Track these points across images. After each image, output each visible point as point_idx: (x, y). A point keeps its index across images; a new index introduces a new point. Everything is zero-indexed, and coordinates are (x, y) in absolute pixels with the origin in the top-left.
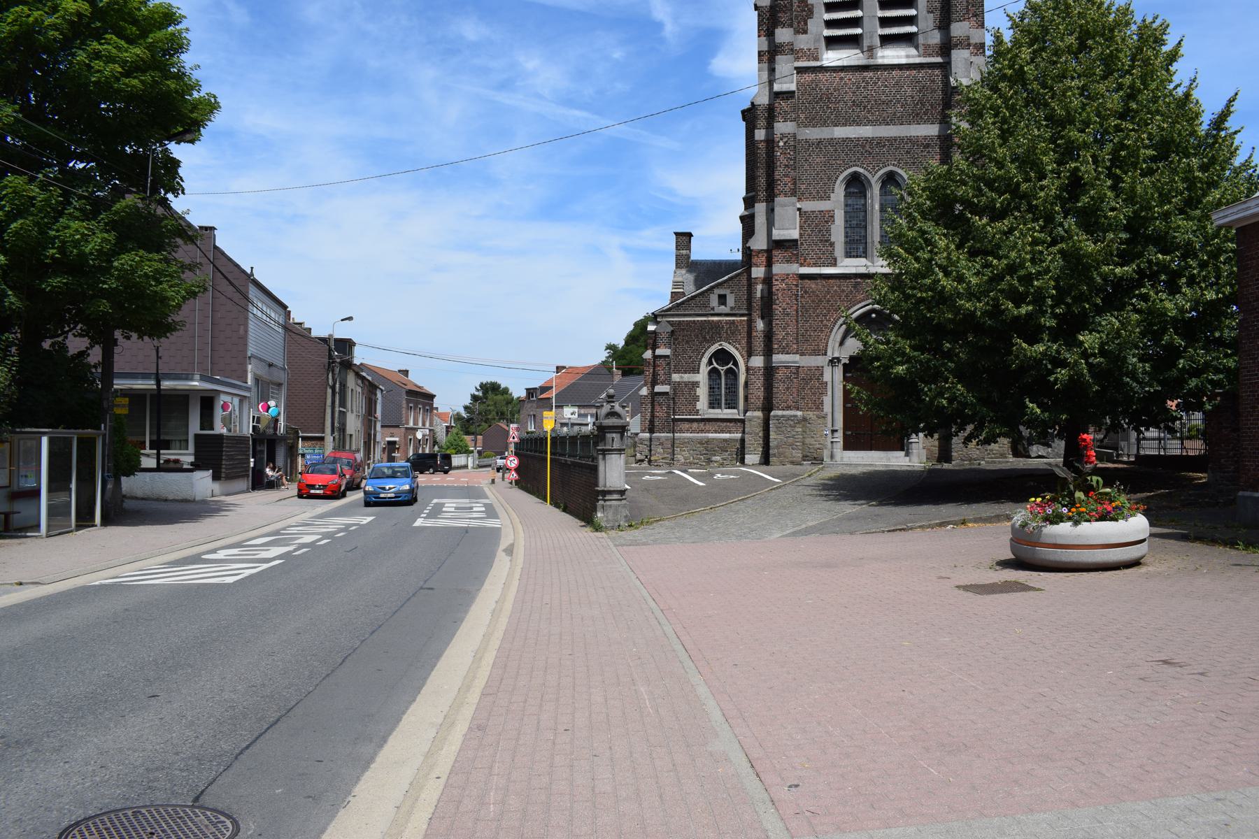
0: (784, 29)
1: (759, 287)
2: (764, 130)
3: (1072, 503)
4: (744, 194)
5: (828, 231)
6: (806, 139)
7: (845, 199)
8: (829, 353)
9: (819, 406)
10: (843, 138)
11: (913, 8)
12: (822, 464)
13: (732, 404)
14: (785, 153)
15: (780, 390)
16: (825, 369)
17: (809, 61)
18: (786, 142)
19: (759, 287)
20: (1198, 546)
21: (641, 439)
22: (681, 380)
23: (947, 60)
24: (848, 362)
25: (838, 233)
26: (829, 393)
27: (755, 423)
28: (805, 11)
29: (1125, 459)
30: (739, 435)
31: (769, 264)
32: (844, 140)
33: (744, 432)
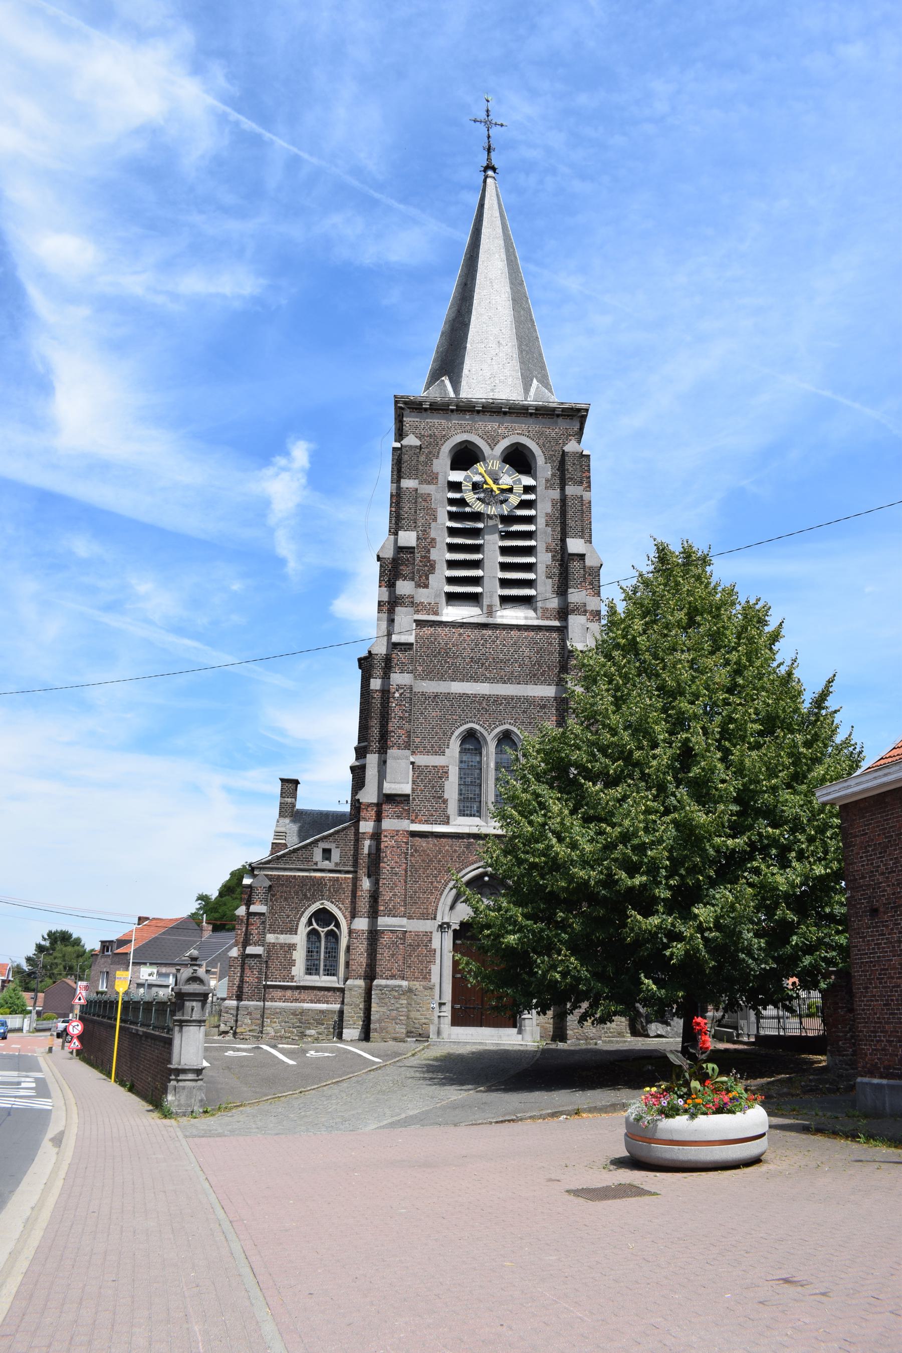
0: (405, 582)
1: (367, 843)
2: (380, 680)
4: (355, 743)
5: (442, 787)
8: (439, 917)
9: (426, 976)
12: (428, 1041)
13: (331, 971)
14: (400, 705)
15: (385, 957)
19: (367, 843)
21: (227, 1008)
22: (276, 941)
23: (564, 624)
24: (458, 928)
25: (451, 790)
26: (438, 961)
28: (426, 566)
29: (745, 1039)
30: (337, 1007)
31: (379, 819)
32: (461, 696)
33: (343, 1003)
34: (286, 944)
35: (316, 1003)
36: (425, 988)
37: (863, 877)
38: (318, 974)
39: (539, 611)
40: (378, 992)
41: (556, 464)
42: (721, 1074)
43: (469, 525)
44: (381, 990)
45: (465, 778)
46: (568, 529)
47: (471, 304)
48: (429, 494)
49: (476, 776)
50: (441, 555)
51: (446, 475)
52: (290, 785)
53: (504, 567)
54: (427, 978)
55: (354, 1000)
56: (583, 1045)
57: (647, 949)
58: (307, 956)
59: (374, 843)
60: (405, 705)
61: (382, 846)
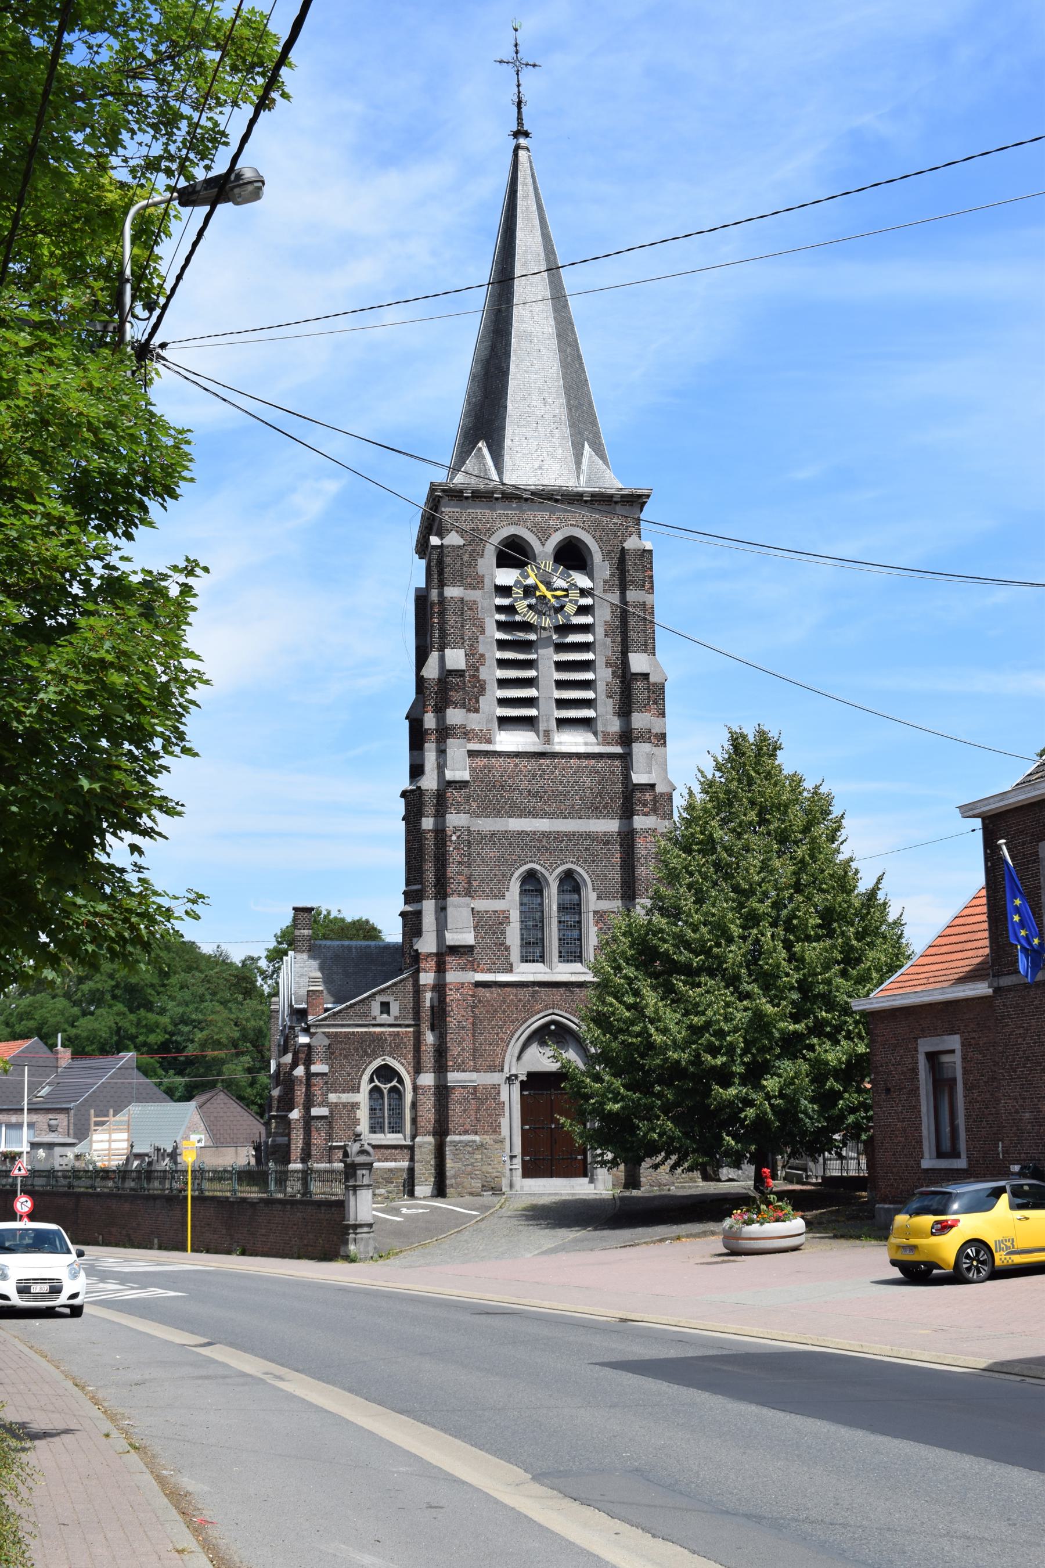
1: (428, 995)
2: (433, 819)
3: (759, 1212)
4: (403, 888)
5: (503, 933)
7: (520, 897)
8: (506, 1069)
9: (496, 1129)
11: (591, 689)
13: (396, 1128)
14: (458, 849)
16: (501, 1087)
18: (460, 836)
19: (428, 995)
20: (842, 1241)
22: (338, 1101)
23: (627, 751)
24: (525, 1079)
25: (513, 935)
26: (507, 1114)
27: (425, 1150)
28: (476, 687)
29: (814, 1180)
30: (405, 1164)
33: (412, 1159)
36: (496, 1142)
37: (882, 1066)
38: (383, 1132)
39: (600, 735)
41: (615, 561)
42: (778, 1201)
43: (521, 636)
45: (526, 922)
46: (630, 642)
47: (508, 344)
48: (475, 601)
51: (493, 577)
53: (561, 684)
55: (425, 1156)
56: (656, 1191)
57: (726, 1113)
58: (370, 1114)
59: (436, 995)
60: (463, 849)
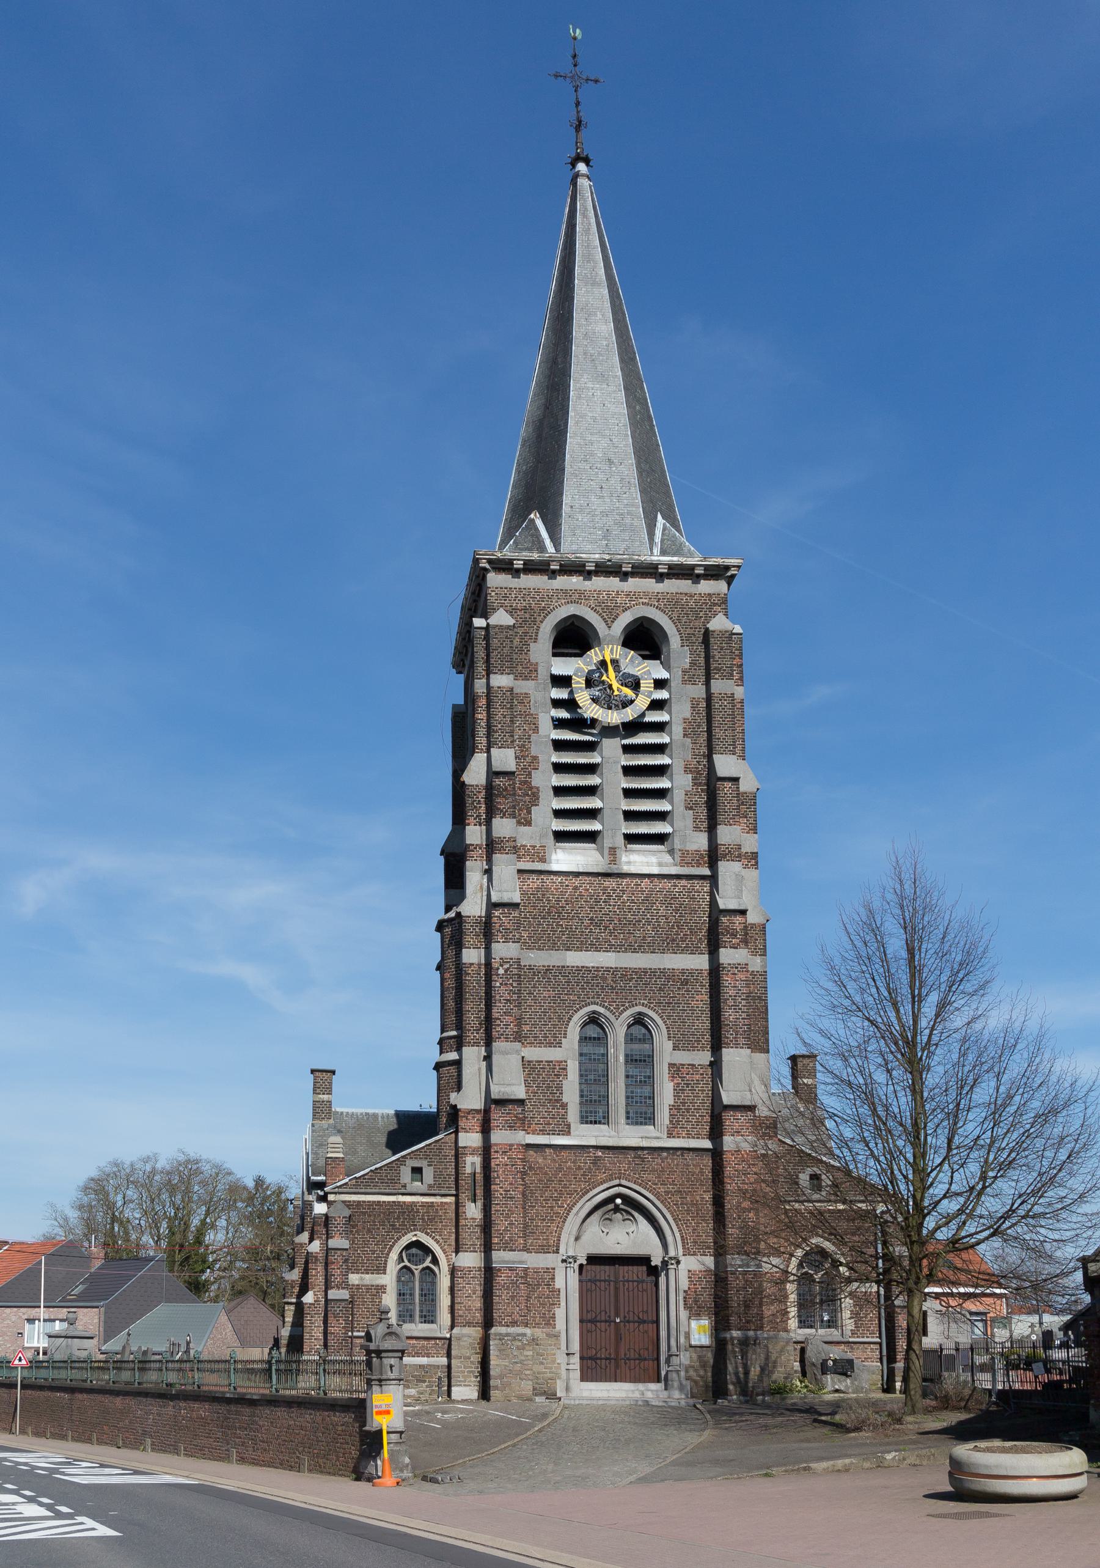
0: (504, 819)
5: (560, 1088)
6: (530, 966)
7: (580, 1046)
8: (562, 1250)
10: (577, 967)
13: (429, 1317)
14: (506, 984)
15: (504, 1300)
17: (533, 861)
22: (361, 1283)
25: (571, 1091)
26: (563, 1304)
28: (528, 795)
31: (486, 1130)
32: (579, 969)
33: (449, 1355)
34: (373, 1286)
35: (413, 1356)
39: (678, 854)
40: (497, 1342)
44: (500, 1339)
49: (600, 1072)
50: (546, 779)
52: (323, 1078)
53: (629, 793)
54: (551, 1324)
60: (512, 984)
61: (493, 1165)
